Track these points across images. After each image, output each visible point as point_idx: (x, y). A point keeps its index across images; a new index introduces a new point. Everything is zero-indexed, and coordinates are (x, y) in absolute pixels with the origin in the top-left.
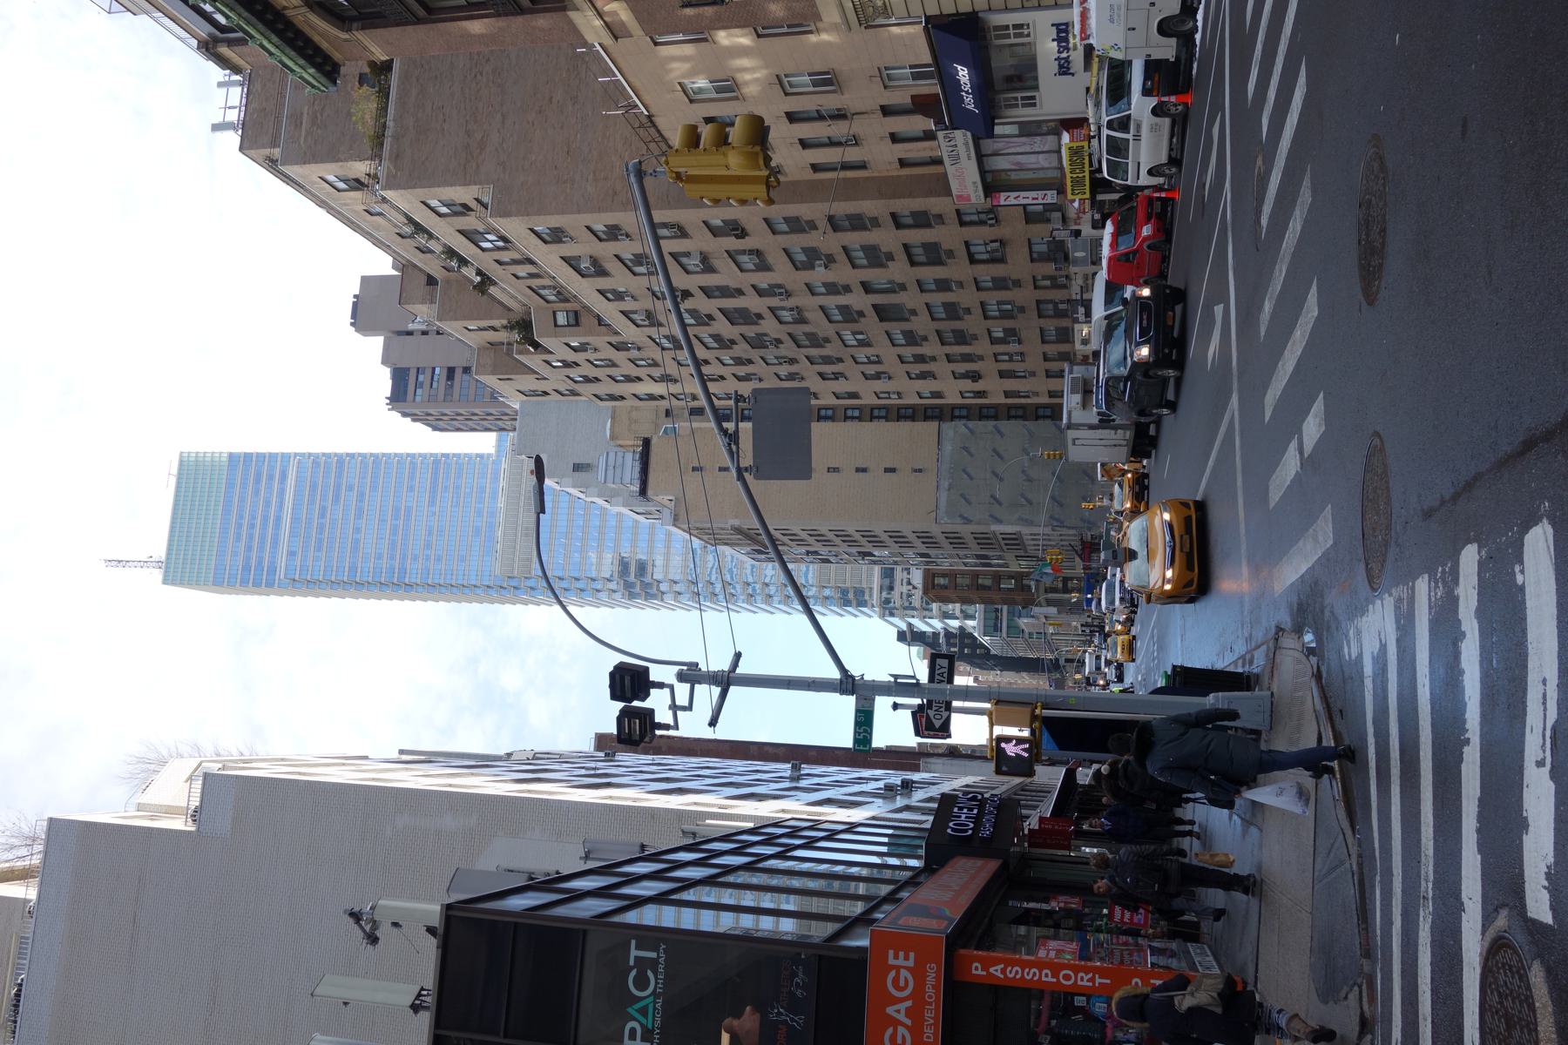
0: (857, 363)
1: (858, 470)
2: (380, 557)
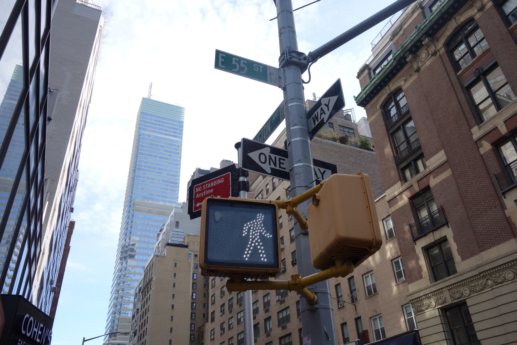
0: (229, 319)
1: (171, 328)
2: (146, 163)
